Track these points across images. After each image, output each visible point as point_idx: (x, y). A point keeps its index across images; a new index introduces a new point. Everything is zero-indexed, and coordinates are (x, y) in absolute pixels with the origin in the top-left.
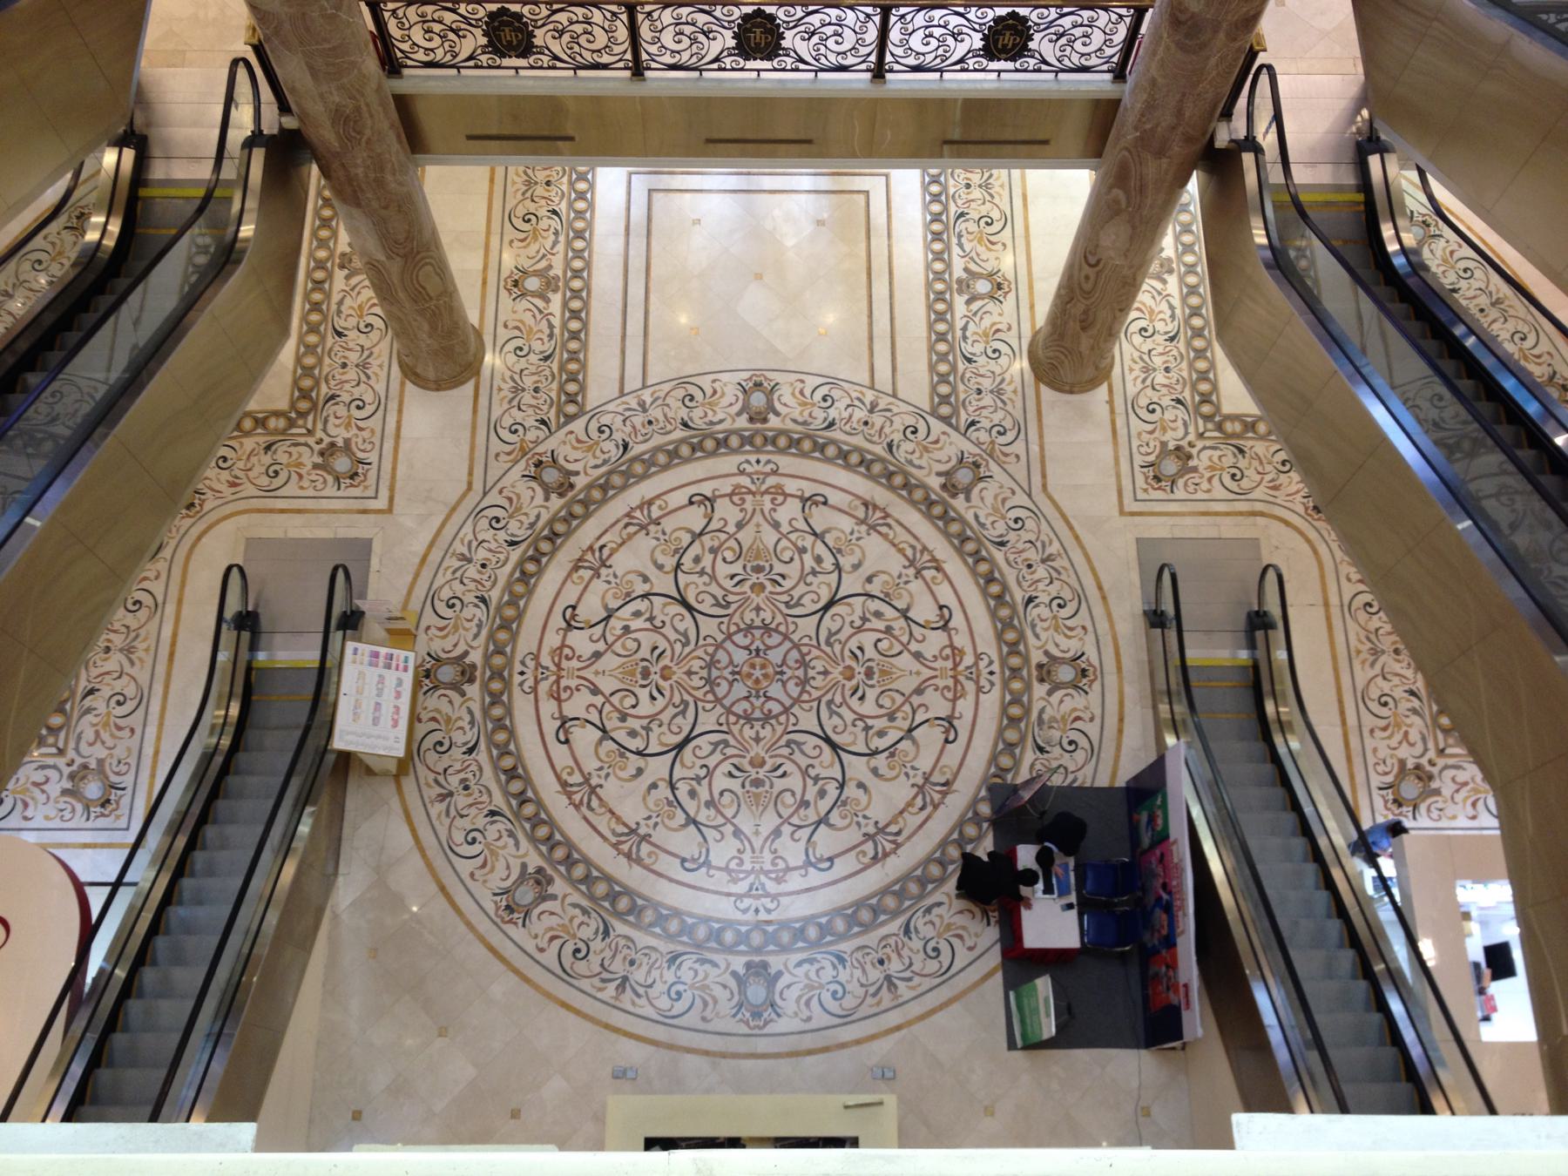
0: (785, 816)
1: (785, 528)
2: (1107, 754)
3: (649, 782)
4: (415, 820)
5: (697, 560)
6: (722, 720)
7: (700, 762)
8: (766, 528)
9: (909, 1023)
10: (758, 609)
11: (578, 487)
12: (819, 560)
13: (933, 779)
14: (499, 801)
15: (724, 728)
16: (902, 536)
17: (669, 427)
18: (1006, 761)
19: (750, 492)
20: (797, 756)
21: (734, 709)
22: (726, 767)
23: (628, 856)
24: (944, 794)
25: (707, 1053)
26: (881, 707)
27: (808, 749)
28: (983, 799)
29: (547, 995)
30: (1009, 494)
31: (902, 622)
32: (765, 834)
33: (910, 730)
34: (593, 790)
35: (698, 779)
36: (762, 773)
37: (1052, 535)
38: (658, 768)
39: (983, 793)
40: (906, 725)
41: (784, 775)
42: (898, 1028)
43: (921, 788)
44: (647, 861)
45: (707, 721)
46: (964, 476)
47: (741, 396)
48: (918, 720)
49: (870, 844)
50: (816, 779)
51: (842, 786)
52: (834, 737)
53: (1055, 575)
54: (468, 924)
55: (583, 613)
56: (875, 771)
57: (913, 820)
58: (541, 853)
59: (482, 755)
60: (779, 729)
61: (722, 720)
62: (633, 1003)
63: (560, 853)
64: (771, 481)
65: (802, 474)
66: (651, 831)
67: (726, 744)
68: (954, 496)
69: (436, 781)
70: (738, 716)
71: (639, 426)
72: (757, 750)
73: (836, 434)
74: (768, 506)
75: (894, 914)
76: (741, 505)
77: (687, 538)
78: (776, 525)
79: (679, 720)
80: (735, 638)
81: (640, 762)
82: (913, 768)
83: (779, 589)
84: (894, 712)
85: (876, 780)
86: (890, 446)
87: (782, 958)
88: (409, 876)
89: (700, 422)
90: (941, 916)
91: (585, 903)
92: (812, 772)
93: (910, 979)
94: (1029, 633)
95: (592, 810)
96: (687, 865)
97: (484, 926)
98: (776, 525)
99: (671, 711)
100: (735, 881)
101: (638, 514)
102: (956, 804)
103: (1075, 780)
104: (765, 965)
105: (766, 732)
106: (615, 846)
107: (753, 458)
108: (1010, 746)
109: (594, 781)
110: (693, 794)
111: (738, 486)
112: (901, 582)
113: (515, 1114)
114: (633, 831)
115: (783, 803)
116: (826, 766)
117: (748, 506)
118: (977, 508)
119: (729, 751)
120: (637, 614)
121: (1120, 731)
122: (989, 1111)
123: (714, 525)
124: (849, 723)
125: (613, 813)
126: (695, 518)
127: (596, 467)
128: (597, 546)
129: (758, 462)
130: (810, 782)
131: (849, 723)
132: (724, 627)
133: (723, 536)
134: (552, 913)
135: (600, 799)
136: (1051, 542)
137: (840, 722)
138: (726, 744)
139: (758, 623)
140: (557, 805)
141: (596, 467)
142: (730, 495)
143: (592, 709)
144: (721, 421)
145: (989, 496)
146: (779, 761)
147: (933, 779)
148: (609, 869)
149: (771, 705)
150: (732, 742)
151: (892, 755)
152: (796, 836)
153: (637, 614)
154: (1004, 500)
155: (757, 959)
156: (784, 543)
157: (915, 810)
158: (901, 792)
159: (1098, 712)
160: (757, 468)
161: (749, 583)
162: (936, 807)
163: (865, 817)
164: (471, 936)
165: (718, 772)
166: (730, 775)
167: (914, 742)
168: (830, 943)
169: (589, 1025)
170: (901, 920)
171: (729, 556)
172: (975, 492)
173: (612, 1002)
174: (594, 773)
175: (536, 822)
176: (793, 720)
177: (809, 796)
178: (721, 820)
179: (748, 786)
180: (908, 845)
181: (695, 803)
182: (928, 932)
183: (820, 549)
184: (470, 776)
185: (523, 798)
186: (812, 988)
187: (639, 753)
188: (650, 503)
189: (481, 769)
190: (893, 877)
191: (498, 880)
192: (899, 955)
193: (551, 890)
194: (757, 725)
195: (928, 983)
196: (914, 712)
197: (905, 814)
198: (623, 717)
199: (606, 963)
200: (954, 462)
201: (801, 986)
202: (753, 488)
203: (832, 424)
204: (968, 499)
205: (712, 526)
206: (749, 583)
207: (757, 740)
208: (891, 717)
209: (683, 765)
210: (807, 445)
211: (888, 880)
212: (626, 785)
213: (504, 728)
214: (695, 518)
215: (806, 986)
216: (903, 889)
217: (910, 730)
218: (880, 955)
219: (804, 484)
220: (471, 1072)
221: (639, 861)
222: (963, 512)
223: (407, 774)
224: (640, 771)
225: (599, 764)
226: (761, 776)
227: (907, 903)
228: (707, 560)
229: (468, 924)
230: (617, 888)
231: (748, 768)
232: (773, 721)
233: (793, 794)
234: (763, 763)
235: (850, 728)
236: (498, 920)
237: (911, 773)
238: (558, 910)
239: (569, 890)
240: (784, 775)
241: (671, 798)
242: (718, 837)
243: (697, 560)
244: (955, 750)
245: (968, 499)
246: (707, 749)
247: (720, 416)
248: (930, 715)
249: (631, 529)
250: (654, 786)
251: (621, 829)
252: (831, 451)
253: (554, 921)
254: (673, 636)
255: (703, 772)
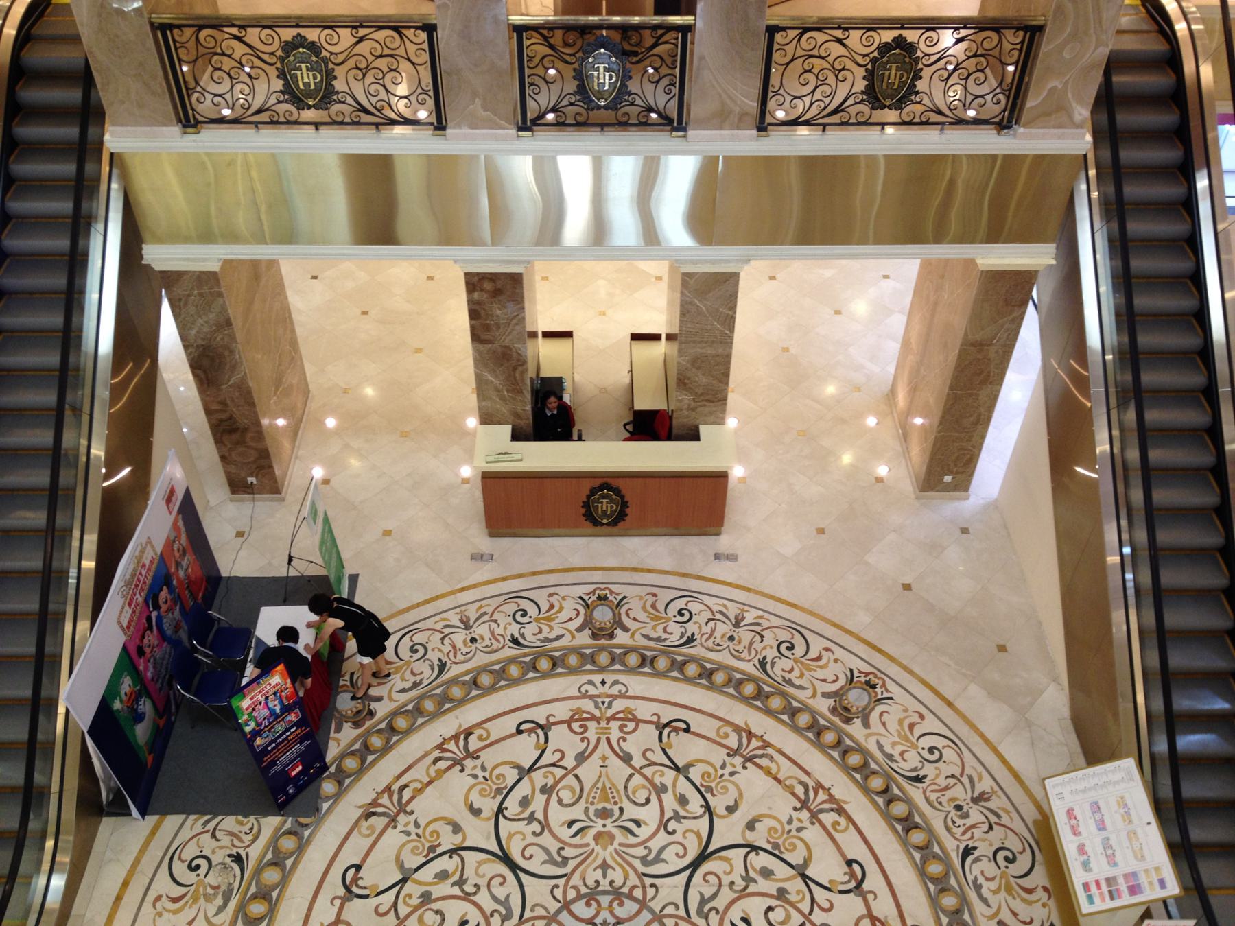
0: (570, 776)
1: (638, 761)
2: (156, 851)
3: (737, 814)
4: (1006, 772)
5: (525, 802)
6: (651, 892)
7: (678, 837)
8: (614, 761)
9: (452, 593)
10: (604, 866)
11: (379, 716)
12: (683, 800)
13: (385, 820)
14: (915, 793)
15: (648, 881)
16: (786, 769)
17: (496, 645)
18: (288, 843)
19: (593, 718)
20: (553, 846)
21: (636, 907)
22: (643, 833)
23: (750, 735)
24: (375, 803)
25: (649, 571)
26: (438, 912)
27: (540, 856)
28: (327, 798)
29: (811, 613)
30: (916, 718)
31: (799, 883)
32: (595, 756)
33: (404, 881)
34: (804, 804)
35: (677, 817)
36: (599, 825)
37: (980, 769)
38: (728, 831)
39: (326, 806)
40: (408, 887)
41: (571, 824)
42: (463, 589)
43: (402, 809)
44: (728, 729)
45: (671, 890)
46: (857, 698)
47: (582, 611)
48: (391, 894)
49: (472, 748)
50: (531, 818)
51: (500, 811)
52: (503, 869)
53: (993, 819)
54: (911, 672)
55: (369, 877)
56: (457, 829)
57: (419, 774)
58: (851, 738)
59: (953, 847)
60: (576, 880)
61: (651, 892)
62: (725, 607)
63: (829, 737)
64: (619, 705)
65: (653, 693)
66: (728, 760)
67: (644, 861)
68: (848, 721)
69: (998, 816)
70: (630, 896)
71: (459, 644)
72: (605, 853)
73: (695, 650)
74: (615, 734)
75: (453, 681)
76: (583, 734)
77: (512, 775)
78: (626, 758)
79: (708, 892)
80: (573, 907)
81: (751, 837)
82: (408, 834)
83: (632, 840)
84: (422, 904)
85: (458, 819)
86: (763, 663)
87: (577, 642)
88: (993, 718)
89: (533, 639)
90: (403, 679)
91: (791, 690)
92: (536, 827)
93: (445, 627)
94: (972, 895)
95: (801, 783)
96: (684, 726)
97: (893, 670)
98: (626, 758)
99: (720, 903)
100: (628, 711)
101: (451, 746)
102: (361, 793)
103: (208, 822)
104: (594, 636)
105: (593, 876)
106: (767, 745)
107: (597, 679)
108: (276, 863)
109: (805, 815)
110: (683, 800)
111: (578, 711)
112: (792, 829)
113: (821, 531)
114: (750, 759)
115: (573, 791)
116: (517, 836)
117: (592, 734)
118: (879, 735)
119: (640, 852)
120: (443, 876)
121: (125, 884)
122: (387, 533)
123: (548, 758)
124: (484, 890)
125: (776, 779)
126: (524, 750)
127: (403, 691)
128: (395, 787)
129: (603, 683)
130: (540, 815)
131: (484, 890)
132: (558, 893)
133: (559, 772)
134: (824, 681)
135: (794, 794)
136: (980, 779)
137: (495, 891)
138: (644, 861)
139: (605, 885)
140: (844, 788)
141: (403, 691)
142: (568, 722)
143: (826, 905)
144: (558, 638)
145: (892, 721)
146: (577, 840)
147: (385, 820)
148: (769, 722)
149: (587, 913)
150: (637, 863)
151: (432, 849)
152: (558, 755)
153: (443, 876)
154: (911, 726)
155: (603, 642)
156: (637, 780)
157: (412, 786)
158: (426, 807)
159: (147, 906)
160: (602, 690)
161: (592, 832)
162: (388, 789)
163: (475, 777)
164: (905, 662)
165: (653, 826)
166: (637, 823)
167: (401, 866)
168: (525, 655)
169: (766, 591)
170: (446, 677)
171: (567, 796)
172: (874, 716)
173: (746, 608)
174: (807, 824)
175: (863, 768)
176: (558, 893)
177: (540, 799)
178: (648, 771)
179: (616, 809)
180: (429, 748)
181: (679, 790)
182: (423, 667)
183: (683, 786)
184: (959, 822)
185: (887, 796)
186: (548, 619)
187: (754, 848)
188: (468, 733)
189: (948, 829)
190: (450, 717)
191: (893, 713)
192: (454, 647)
193: (831, 702)
194: (605, 885)
195: (429, 624)
196: (395, 904)
197: (426, 780)
198: (782, 894)
199: (758, 638)
200: (842, 681)
201: (557, 620)
202: (597, 713)
203: (691, 640)
204: (866, 724)
205: (546, 760)
206: (592, 832)
207: (604, 866)
208: (426, 898)
209: (698, 834)
210: (662, 663)
211: (457, 712)
212: (766, 811)
213: (934, 880)
214: (524, 750)
215: (553, 620)
216: (441, 704)
217: (404, 881)
218: (474, 646)
219: (656, 708)
220: (871, 559)
221: (737, 729)
222: (861, 740)
223: (1035, 822)
224: (751, 826)
225: (803, 834)
226: (600, 822)
227: (438, 691)
228: (538, 802)
229: (911, 672)
230: (758, 703)
231: (615, 831)
232: (584, 890)
233: (560, 802)
234: (597, 837)
235: (483, 882)
236: (880, 675)
237: (411, 828)
238: (818, 684)
239: (810, 702)
240: (571, 824)
241: (708, 796)
242: (649, 754)
243: (525, 802)
244: (350, 856)
245: (866, 724)
246: (668, 854)
247: (558, 631)
248: (373, 902)
249: (442, 765)
250: (731, 810)
251: (764, 762)
252: (692, 670)
253: (820, 674)
254: (489, 905)
255: (672, 826)
